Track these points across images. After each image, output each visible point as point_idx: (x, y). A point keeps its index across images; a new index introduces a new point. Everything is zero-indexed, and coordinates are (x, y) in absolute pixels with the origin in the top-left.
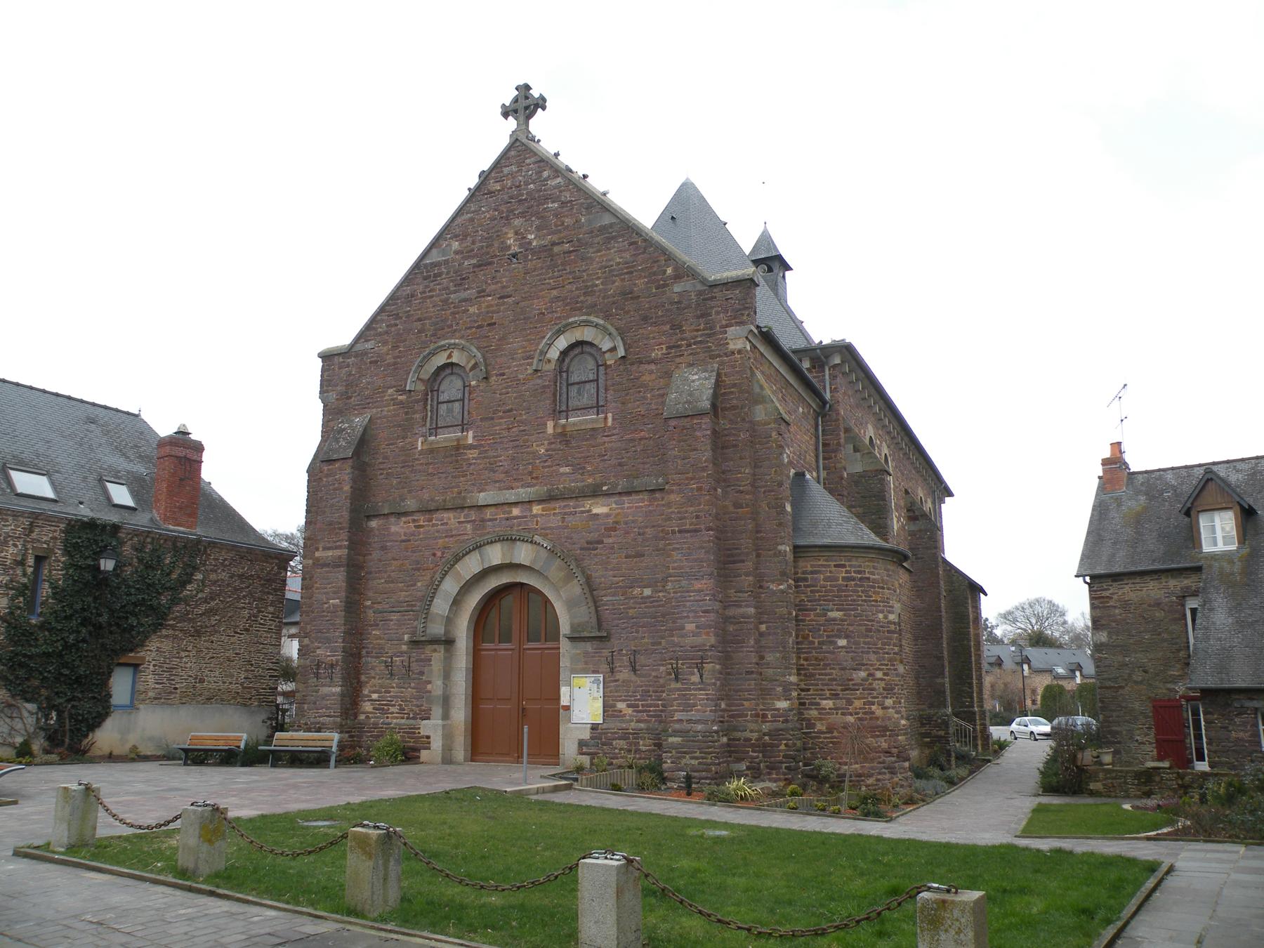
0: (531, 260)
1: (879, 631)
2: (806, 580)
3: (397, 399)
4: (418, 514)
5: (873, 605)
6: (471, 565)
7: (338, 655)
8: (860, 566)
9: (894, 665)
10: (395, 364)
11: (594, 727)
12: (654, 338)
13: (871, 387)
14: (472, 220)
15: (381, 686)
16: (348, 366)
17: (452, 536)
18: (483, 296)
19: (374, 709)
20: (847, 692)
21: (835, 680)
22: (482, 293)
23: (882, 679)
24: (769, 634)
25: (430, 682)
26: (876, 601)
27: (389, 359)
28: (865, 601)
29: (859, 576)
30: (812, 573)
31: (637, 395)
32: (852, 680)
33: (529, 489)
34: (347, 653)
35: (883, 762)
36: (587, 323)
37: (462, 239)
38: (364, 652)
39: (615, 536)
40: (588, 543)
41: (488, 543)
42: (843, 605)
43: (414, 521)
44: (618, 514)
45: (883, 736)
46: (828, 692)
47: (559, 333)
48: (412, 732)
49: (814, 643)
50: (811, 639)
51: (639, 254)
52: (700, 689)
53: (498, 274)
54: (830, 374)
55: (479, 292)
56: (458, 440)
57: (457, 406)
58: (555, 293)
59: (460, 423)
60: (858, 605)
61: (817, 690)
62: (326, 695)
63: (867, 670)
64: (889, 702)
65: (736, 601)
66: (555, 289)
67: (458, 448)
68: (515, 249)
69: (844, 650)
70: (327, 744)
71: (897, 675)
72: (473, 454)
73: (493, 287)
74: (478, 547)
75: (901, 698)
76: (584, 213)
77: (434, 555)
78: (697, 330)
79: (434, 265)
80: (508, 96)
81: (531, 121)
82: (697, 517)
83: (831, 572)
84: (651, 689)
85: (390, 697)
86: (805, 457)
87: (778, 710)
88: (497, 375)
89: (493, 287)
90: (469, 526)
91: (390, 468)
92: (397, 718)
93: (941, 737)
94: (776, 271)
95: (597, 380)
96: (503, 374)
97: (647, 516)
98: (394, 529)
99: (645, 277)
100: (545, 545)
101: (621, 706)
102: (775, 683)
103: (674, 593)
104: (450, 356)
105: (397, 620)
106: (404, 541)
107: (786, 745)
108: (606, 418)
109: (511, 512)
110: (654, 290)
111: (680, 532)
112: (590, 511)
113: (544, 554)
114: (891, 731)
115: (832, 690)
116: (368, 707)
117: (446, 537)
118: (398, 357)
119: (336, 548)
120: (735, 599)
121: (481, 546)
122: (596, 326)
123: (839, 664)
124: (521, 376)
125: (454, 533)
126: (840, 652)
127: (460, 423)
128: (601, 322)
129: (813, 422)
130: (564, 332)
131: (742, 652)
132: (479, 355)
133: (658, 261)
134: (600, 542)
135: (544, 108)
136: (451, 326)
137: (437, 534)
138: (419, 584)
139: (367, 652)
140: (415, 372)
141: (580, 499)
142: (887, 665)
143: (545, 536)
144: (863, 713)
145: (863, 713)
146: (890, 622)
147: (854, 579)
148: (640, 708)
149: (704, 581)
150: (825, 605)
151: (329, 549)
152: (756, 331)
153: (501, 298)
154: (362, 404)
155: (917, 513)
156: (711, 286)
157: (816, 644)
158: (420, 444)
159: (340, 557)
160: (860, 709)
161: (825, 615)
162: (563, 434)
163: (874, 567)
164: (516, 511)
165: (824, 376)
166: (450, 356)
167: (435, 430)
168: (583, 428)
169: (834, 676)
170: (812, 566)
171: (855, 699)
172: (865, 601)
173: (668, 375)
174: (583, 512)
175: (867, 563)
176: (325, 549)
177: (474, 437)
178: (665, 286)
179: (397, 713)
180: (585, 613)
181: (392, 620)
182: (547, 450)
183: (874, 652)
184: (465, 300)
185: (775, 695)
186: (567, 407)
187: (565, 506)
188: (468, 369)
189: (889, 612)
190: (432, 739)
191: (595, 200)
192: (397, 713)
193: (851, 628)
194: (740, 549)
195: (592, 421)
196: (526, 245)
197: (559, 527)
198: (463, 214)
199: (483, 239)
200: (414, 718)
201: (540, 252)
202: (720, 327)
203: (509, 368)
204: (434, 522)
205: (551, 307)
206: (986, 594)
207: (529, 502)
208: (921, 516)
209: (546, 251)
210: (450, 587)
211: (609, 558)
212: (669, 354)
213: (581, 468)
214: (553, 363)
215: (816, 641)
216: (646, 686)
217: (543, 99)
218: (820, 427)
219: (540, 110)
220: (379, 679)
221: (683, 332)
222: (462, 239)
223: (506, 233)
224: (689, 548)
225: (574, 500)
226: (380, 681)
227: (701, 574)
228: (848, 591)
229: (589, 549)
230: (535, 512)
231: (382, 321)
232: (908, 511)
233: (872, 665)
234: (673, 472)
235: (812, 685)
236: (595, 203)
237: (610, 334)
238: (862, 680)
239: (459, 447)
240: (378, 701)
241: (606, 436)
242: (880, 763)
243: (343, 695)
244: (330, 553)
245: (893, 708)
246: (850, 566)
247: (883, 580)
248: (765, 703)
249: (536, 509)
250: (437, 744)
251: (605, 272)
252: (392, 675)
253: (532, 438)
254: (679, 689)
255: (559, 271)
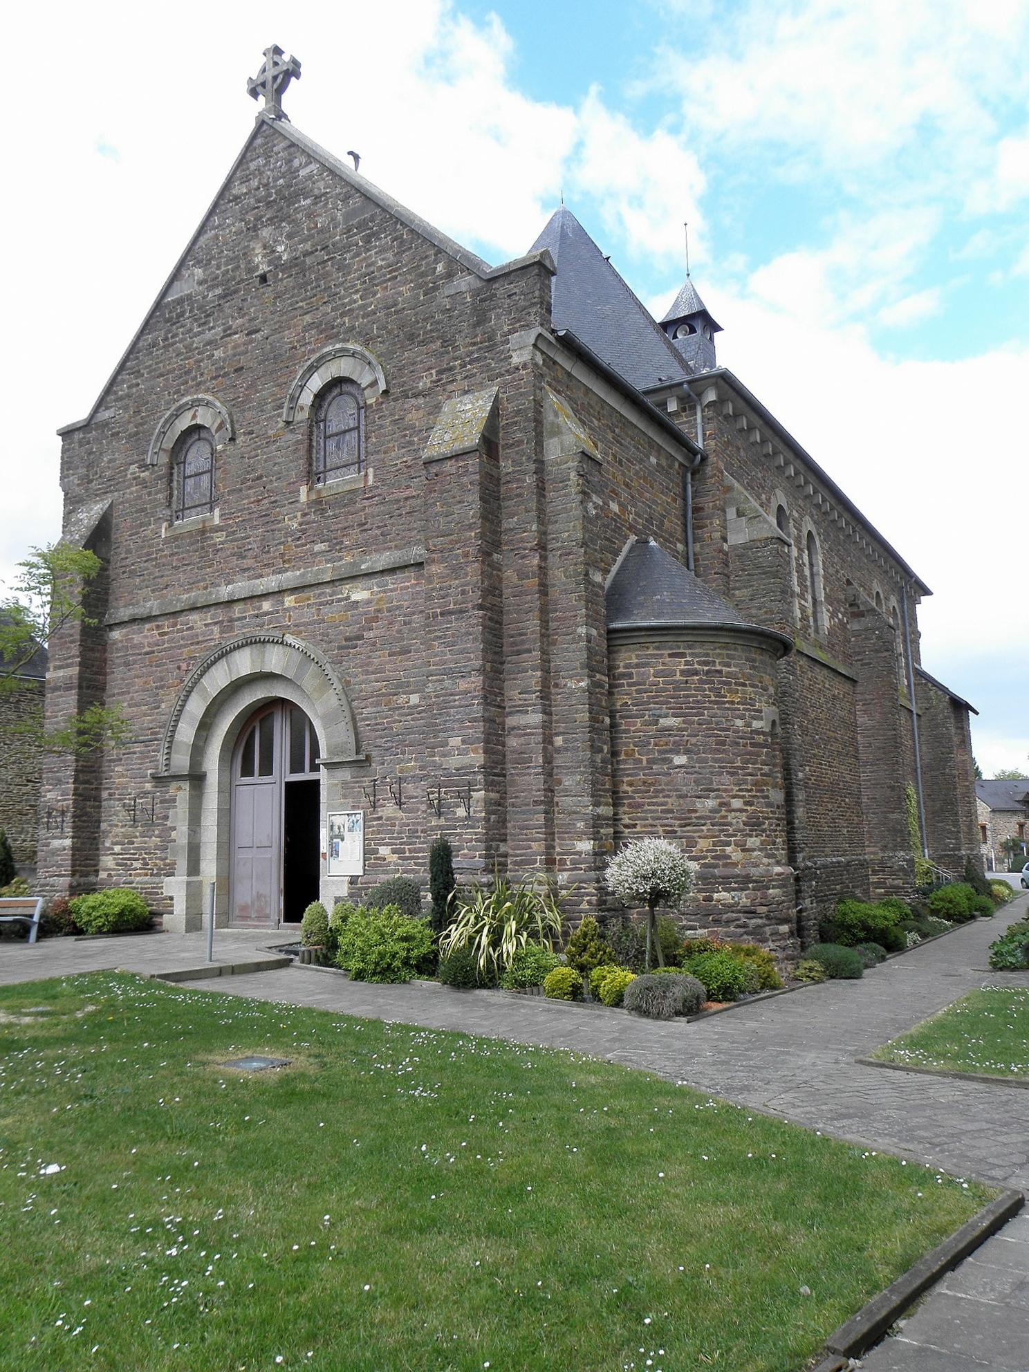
0: (282, 280)
1: (738, 744)
2: (630, 676)
3: (139, 477)
4: (162, 618)
5: (728, 709)
6: (218, 679)
7: (68, 800)
8: (707, 655)
9: (762, 791)
10: (137, 433)
11: (353, 880)
12: (421, 362)
13: (777, 439)
14: (217, 237)
15: (124, 836)
16: (88, 443)
17: (198, 643)
18: (230, 335)
19: (117, 864)
20: (689, 828)
21: (671, 811)
22: (228, 332)
23: (741, 811)
24: (566, 749)
25: (174, 829)
26: (732, 702)
27: (132, 429)
28: (716, 703)
29: (706, 668)
30: (638, 666)
31: (403, 440)
32: (696, 811)
33: (279, 576)
34: (80, 795)
35: (745, 926)
36: (344, 353)
37: (206, 265)
38: (105, 794)
39: (377, 628)
40: (347, 639)
41: (235, 649)
42: (682, 708)
43: (158, 627)
44: (380, 600)
45: (742, 890)
46: (661, 829)
47: (312, 369)
48: (154, 891)
49: (640, 761)
50: (637, 756)
51: (404, 251)
52: (469, 827)
53: (245, 304)
54: (703, 417)
55: (225, 331)
56: (204, 522)
57: (205, 479)
58: (308, 318)
59: (208, 500)
60: (705, 708)
61: (645, 826)
62: (58, 850)
63: (717, 797)
64: (753, 842)
65: (520, 706)
66: (308, 313)
67: (203, 532)
68: (264, 268)
69: (683, 770)
70: (27, 911)
71: (769, 805)
72: (219, 537)
73: (240, 321)
74: (224, 654)
75: (776, 836)
76: (340, 207)
77: (179, 668)
78: (474, 344)
79: (180, 301)
80: (253, 66)
81: (283, 97)
82: (463, 592)
83: (663, 664)
84: (419, 828)
85: (133, 849)
86: (662, 523)
87: (579, 853)
88: (245, 434)
89: (240, 321)
90: (216, 629)
91: (133, 565)
92: (140, 875)
93: (898, 887)
94: (699, 331)
95: (358, 427)
96: (251, 433)
97: (413, 599)
98: (137, 639)
99: (411, 282)
100: (297, 646)
101: (384, 851)
102: (574, 816)
103: (435, 697)
104: (194, 417)
105: (141, 752)
106: (147, 653)
107: (589, 902)
108: (366, 475)
109: (260, 608)
110: (422, 298)
111: (442, 614)
112: (348, 598)
113: (297, 657)
114: (756, 881)
115: (666, 825)
116: (108, 861)
117: (192, 644)
118: (141, 424)
119: (68, 666)
120: (521, 703)
121: (227, 653)
122: (354, 355)
123: (677, 790)
124: (271, 432)
125: (200, 639)
126: (678, 773)
127: (208, 500)
128: (358, 348)
129: (678, 480)
130: (317, 368)
131: (529, 774)
132: (224, 411)
133: (426, 257)
134: (360, 638)
135: (298, 77)
136: (194, 378)
137: (182, 642)
138: (163, 706)
139: (110, 795)
140: (157, 441)
141: (337, 584)
142: (751, 791)
143: (297, 634)
144: (713, 857)
145: (713, 857)
146: (757, 732)
147: (696, 673)
148: (407, 854)
149: (472, 679)
150: (655, 709)
151: (60, 667)
152: (551, 337)
153: (247, 335)
154: (103, 488)
155: (862, 608)
156: (489, 280)
157: (645, 762)
158: (163, 530)
159: (71, 677)
160: (708, 851)
161: (656, 723)
162: (318, 502)
163: (728, 656)
164: (266, 606)
165: (695, 420)
166: (194, 417)
167: (180, 513)
168: (340, 490)
169: (669, 807)
170: (638, 657)
171: (700, 837)
172: (716, 703)
173: (437, 408)
174: (340, 600)
175: (718, 651)
176: (56, 668)
177: (221, 516)
178: (435, 288)
179: (141, 869)
180: (344, 734)
181: (135, 753)
182: (301, 524)
183: (728, 773)
184: (210, 343)
185: (576, 832)
186: (325, 467)
187: (320, 595)
188: (213, 431)
189: (754, 718)
190: (174, 902)
191: (353, 186)
192: (141, 869)
193: (694, 740)
194: (526, 634)
195: (354, 481)
196: (275, 261)
197: (314, 622)
198: (206, 232)
199: (230, 260)
200: (158, 875)
201: (291, 267)
202: (502, 336)
203: (258, 423)
204: (179, 627)
205: (304, 338)
206: (977, 713)
207: (280, 592)
208: (868, 611)
209: (295, 262)
210: (196, 707)
211: (369, 657)
212: (439, 380)
213: (337, 544)
214: (307, 410)
215: (644, 758)
216: (414, 824)
217: (296, 63)
218: (689, 486)
219: (293, 79)
220: (122, 827)
221: (456, 348)
222: (206, 265)
223: (253, 249)
224: (453, 635)
225: (331, 585)
226: (123, 830)
227: (468, 669)
228: (689, 689)
229: (347, 647)
230: (287, 604)
231: (123, 381)
232: (851, 605)
233: (725, 791)
234: (434, 534)
235: (639, 819)
236: (353, 191)
237: (369, 363)
238: (711, 811)
239: (204, 532)
240: (121, 854)
241: (367, 499)
242: (740, 927)
243: (74, 848)
244: (61, 673)
245: (760, 850)
246: (692, 655)
247: (743, 674)
248: (562, 845)
249: (289, 601)
250: (180, 907)
251: (365, 282)
252: (134, 821)
253: (284, 510)
254: (440, 828)
255: (312, 289)
